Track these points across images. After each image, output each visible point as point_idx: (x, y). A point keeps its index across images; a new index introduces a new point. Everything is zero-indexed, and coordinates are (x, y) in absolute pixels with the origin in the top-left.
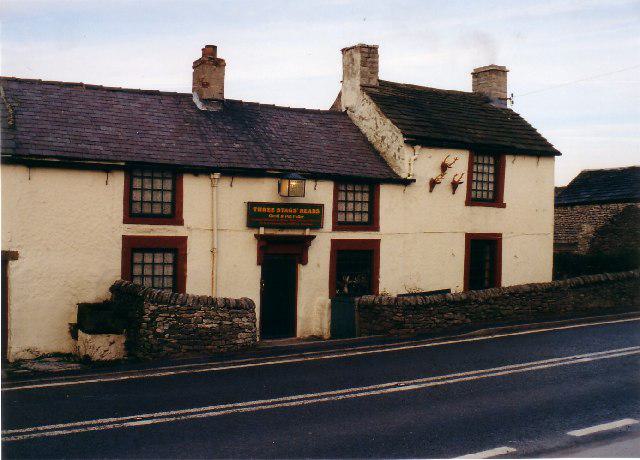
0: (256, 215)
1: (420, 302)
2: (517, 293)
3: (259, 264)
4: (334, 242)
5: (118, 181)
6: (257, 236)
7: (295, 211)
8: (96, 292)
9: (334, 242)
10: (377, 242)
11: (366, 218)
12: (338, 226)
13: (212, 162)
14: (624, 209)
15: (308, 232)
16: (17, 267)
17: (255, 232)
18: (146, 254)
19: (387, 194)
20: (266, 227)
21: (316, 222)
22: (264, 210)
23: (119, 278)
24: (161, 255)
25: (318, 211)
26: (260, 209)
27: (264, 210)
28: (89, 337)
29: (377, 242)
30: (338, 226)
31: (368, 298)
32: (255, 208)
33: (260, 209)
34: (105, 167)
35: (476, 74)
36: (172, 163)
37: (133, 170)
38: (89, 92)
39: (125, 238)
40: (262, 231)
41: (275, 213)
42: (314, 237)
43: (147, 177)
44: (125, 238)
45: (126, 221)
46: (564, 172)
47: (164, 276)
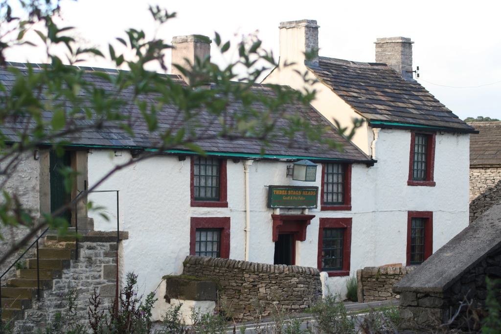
0: (273, 196)
3: (273, 241)
5: (186, 165)
6: (274, 217)
8: (176, 269)
10: (349, 221)
11: (325, 201)
14: (284, 94)
15: (307, 212)
18: (209, 233)
19: (357, 173)
23: (188, 255)
24: (211, 233)
25: (475, 162)
29: (349, 221)
34: (181, 158)
37: (198, 160)
40: (278, 212)
41: (287, 196)
43: (202, 165)
45: (193, 205)
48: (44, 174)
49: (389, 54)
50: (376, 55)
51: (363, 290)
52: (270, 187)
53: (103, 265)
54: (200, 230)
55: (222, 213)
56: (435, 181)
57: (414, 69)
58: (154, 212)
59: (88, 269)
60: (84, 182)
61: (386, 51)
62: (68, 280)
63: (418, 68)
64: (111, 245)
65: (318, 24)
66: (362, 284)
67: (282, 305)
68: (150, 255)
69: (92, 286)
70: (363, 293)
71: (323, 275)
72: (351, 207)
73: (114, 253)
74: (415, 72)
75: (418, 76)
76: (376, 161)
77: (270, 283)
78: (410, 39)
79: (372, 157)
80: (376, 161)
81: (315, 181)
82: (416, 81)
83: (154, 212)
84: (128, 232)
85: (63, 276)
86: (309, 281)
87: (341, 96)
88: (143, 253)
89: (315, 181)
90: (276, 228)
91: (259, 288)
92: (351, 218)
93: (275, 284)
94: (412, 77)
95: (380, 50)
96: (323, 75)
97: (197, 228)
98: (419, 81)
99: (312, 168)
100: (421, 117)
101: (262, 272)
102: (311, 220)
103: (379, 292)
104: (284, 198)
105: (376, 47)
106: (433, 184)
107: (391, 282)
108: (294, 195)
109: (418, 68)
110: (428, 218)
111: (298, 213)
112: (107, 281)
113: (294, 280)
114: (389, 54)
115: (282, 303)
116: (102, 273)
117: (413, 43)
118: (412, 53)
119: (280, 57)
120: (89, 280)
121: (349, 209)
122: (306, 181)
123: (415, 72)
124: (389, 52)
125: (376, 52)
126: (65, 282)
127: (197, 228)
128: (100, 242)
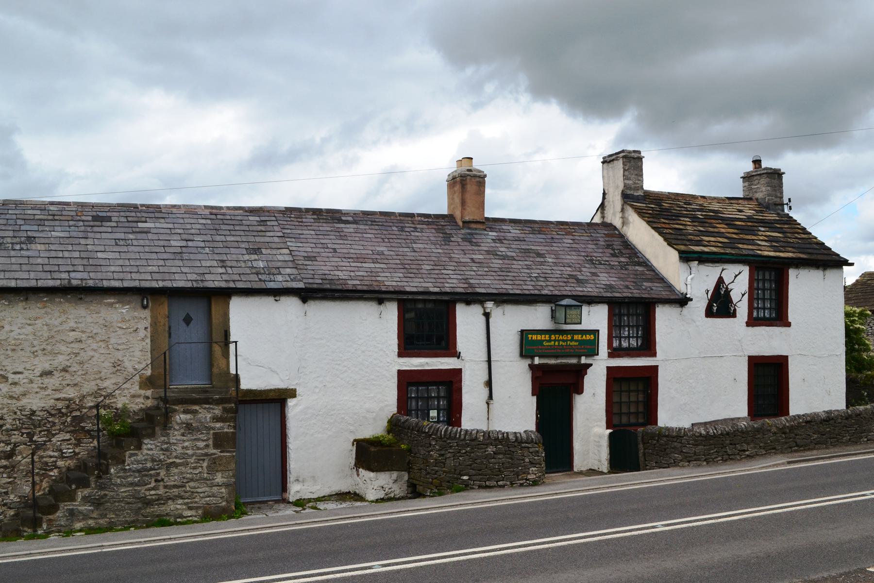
1: (703, 432)
2: (811, 422)
4: (609, 369)
6: (532, 367)
7: (569, 337)
9: (609, 369)
10: (655, 368)
12: (614, 353)
13: (279, 282)
15: (584, 360)
16: (296, 405)
17: (529, 362)
19: (664, 317)
20: (540, 356)
21: (593, 352)
22: (539, 337)
25: (592, 337)
26: (534, 337)
27: (539, 337)
28: (372, 475)
29: (655, 368)
30: (614, 353)
31: (650, 428)
32: (530, 336)
33: (534, 337)
35: (603, 158)
36: (201, 285)
38: (536, 242)
39: (400, 373)
40: (537, 361)
41: (550, 341)
42: (591, 365)
44: (400, 373)
46: (850, 275)
47: (630, 402)
48: (158, 324)
49: (756, 187)
50: (743, 190)
51: (644, 454)
52: (522, 331)
53: (212, 432)
54: (411, 384)
55: (448, 364)
56: (790, 320)
57: (786, 201)
58: (339, 365)
59: (185, 438)
60: (223, 332)
61: (752, 184)
62: (150, 452)
63: (790, 200)
64: (223, 407)
65: (642, 154)
66: (643, 447)
67: (474, 481)
68: (332, 415)
69: (194, 458)
70: (645, 458)
71: (53, 502)
72: (656, 353)
73: (232, 417)
74: (787, 204)
75: (790, 208)
76: (691, 300)
77: (458, 453)
78: (780, 170)
79: (686, 294)
80: (691, 300)
81: (581, 323)
82: (788, 214)
83: (339, 365)
84: (295, 389)
85: (145, 447)
86: (513, 450)
87: (653, 228)
88: (320, 413)
89: (581, 323)
90: (534, 380)
91: (446, 458)
92: (658, 366)
93: (465, 453)
94: (783, 210)
95: (746, 184)
96: (792, 222)
97: (407, 383)
98: (792, 214)
99: (575, 309)
100: (762, 248)
101: (450, 438)
102: (588, 370)
103: (660, 457)
104: (545, 344)
105: (744, 182)
106: (788, 325)
107: (672, 446)
108: (561, 340)
109: (790, 200)
110: (782, 363)
111: (574, 361)
112: (220, 452)
113: (491, 450)
114: (756, 187)
115: (474, 478)
116: (211, 442)
117: (784, 173)
118: (782, 184)
119: (604, 194)
120: (188, 452)
121: (654, 354)
122: (566, 323)
123: (787, 204)
124: (756, 185)
125: (743, 187)
126: (147, 454)
127: (407, 383)
128: (206, 404)
